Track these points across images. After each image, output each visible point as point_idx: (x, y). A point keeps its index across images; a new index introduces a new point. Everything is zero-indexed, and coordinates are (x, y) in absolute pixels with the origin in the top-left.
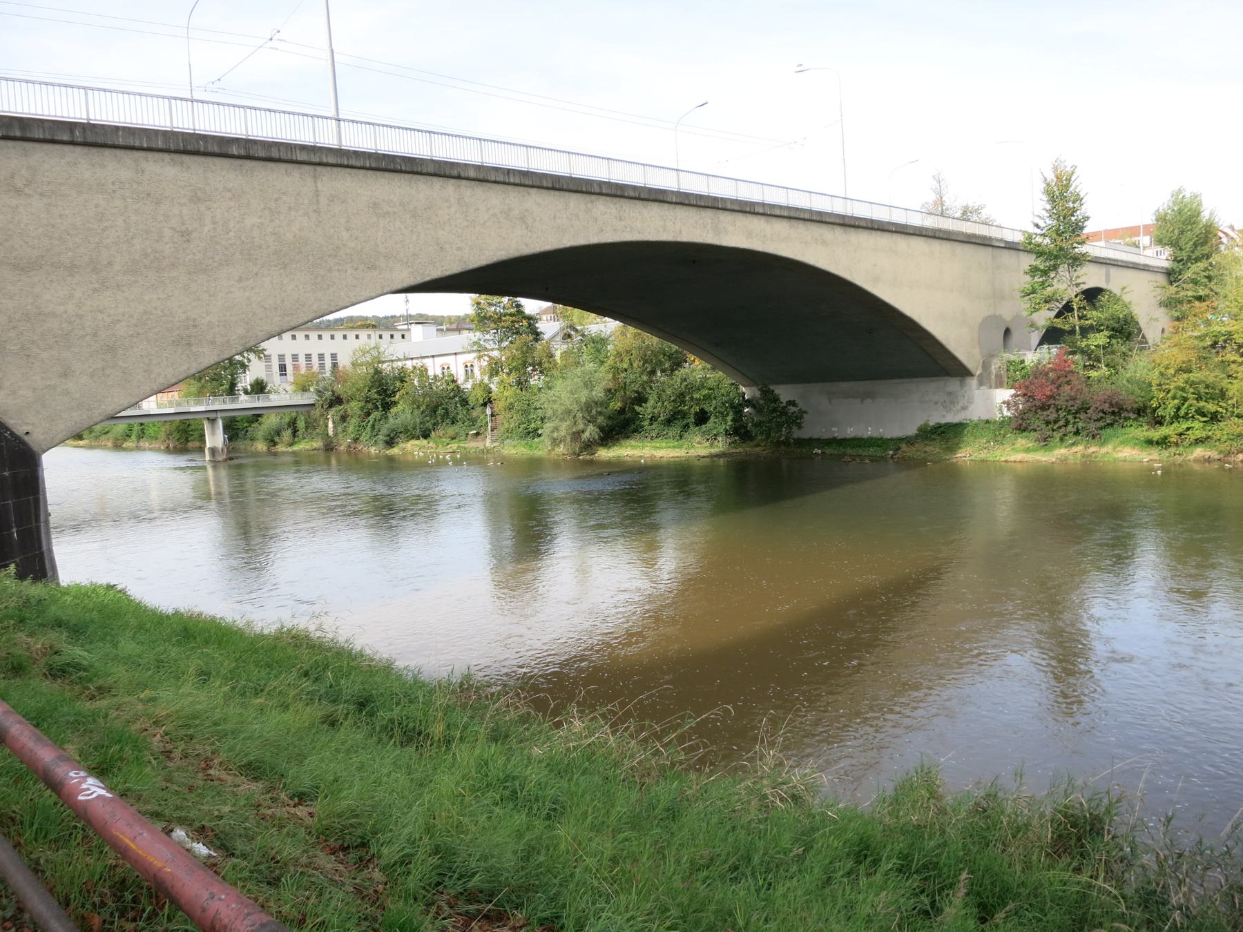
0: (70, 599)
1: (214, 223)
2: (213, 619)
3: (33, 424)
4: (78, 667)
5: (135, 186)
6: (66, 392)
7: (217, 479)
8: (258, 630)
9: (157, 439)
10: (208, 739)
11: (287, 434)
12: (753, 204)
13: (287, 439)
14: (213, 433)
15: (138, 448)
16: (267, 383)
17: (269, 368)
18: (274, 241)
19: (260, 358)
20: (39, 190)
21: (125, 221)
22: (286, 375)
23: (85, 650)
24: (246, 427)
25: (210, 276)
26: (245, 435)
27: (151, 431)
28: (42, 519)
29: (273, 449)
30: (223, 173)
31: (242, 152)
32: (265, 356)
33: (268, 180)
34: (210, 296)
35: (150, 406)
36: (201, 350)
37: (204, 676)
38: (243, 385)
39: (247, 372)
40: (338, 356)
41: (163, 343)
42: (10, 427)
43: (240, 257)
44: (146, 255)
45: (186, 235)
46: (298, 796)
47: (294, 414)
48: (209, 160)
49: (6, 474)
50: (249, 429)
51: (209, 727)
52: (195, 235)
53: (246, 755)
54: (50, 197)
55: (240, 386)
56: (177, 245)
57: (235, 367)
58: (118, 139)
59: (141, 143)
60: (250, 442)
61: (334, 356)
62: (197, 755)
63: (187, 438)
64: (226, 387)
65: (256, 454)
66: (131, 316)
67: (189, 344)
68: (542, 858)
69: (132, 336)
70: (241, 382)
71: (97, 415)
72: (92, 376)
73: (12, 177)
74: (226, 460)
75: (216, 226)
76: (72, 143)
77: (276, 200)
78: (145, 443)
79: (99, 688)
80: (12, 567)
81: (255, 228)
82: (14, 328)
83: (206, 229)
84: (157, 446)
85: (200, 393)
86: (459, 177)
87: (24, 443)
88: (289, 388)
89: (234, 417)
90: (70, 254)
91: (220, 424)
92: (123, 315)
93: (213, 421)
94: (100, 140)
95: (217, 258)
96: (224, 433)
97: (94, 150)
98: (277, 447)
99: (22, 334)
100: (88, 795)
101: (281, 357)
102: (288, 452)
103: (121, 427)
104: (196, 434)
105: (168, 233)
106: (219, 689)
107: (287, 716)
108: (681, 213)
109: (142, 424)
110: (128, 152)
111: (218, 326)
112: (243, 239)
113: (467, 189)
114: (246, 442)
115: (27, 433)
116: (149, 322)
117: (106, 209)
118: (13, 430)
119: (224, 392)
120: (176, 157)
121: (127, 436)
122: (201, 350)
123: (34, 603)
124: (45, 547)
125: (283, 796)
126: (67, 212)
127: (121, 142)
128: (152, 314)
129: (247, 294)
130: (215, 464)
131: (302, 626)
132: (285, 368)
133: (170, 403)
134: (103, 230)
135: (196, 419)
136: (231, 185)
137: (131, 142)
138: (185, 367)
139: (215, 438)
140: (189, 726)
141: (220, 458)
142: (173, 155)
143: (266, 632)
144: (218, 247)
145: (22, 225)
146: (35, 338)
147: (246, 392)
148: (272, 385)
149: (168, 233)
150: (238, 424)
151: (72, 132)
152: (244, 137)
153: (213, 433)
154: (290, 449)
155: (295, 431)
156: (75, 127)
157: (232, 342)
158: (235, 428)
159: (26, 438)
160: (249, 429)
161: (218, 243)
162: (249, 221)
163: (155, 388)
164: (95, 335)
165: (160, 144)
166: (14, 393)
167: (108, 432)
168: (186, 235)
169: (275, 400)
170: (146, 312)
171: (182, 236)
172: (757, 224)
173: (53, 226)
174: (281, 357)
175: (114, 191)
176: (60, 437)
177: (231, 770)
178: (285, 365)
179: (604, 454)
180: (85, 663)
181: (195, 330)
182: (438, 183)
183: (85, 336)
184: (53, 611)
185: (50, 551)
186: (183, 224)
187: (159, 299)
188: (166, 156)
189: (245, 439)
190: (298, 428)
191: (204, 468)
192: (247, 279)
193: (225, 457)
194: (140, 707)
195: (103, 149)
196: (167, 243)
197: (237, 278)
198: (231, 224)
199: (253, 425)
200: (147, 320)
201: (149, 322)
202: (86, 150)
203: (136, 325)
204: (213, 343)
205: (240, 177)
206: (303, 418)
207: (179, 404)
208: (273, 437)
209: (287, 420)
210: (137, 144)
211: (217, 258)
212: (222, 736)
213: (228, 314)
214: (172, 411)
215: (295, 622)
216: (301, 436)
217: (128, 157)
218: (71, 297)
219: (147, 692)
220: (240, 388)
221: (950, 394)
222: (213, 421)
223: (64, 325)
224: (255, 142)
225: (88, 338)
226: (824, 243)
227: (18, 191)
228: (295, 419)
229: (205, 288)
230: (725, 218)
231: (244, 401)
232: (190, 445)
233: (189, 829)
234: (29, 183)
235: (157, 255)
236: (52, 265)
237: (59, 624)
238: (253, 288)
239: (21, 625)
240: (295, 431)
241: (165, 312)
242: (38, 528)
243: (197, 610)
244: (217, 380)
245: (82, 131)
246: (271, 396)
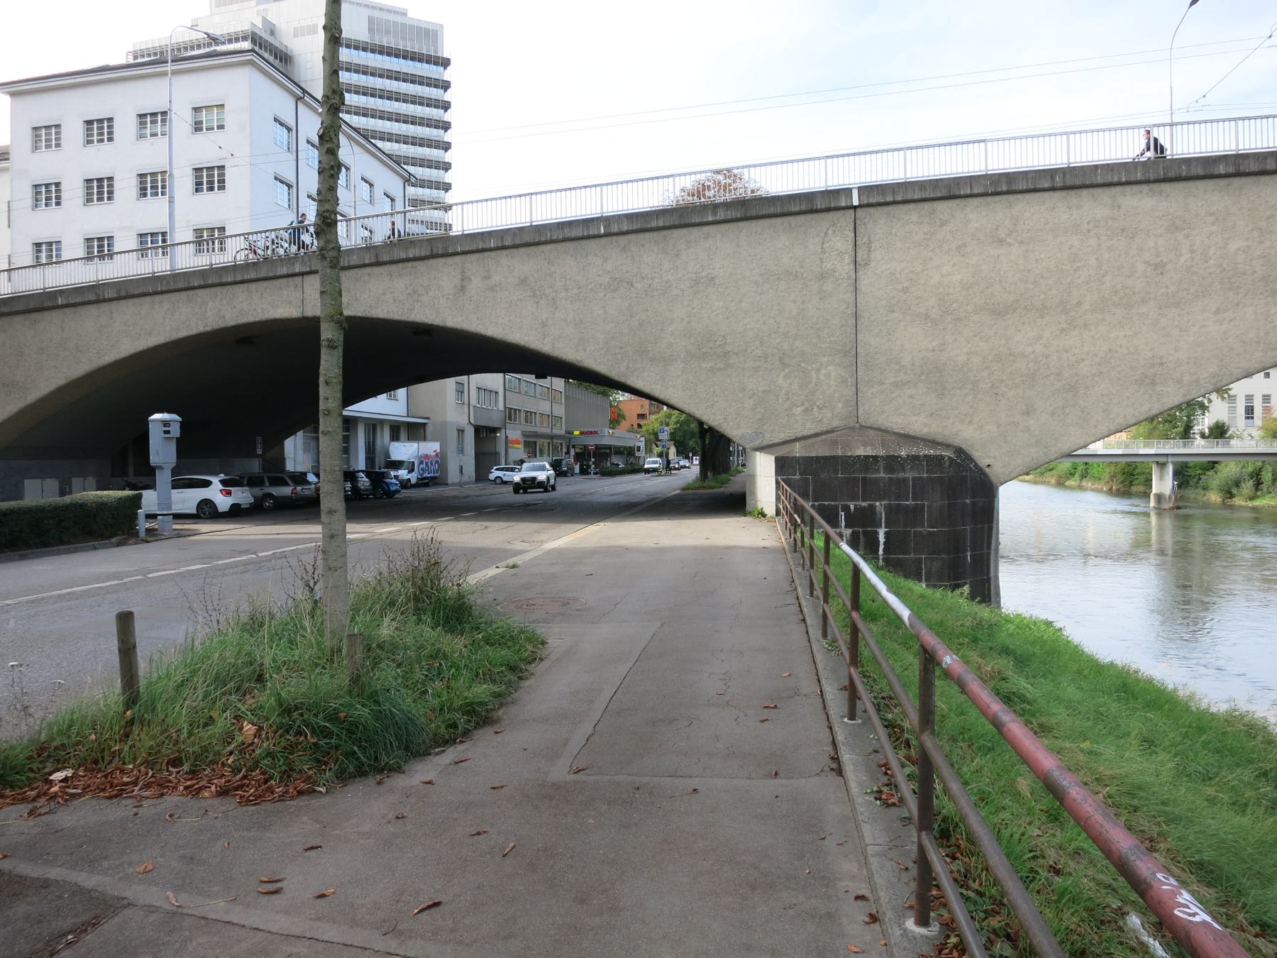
0: (1013, 627)
1: (1192, 252)
2: (1150, 681)
3: (994, 458)
4: (1023, 699)
5: (1110, 222)
6: (1028, 429)
7: (1160, 529)
8: (1204, 705)
9: (1100, 479)
10: (1154, 817)
11: (1248, 486)
13: (1248, 491)
14: (1161, 478)
15: (1081, 488)
16: (1229, 427)
17: (1232, 410)
18: (1262, 265)
19: (1223, 398)
20: (1020, 238)
21: (1097, 259)
22: (1252, 418)
23: (1029, 683)
24: (1199, 475)
25: (1183, 310)
26: (1197, 483)
27: (1094, 471)
28: (993, 547)
29: (1229, 502)
30: (1206, 197)
31: (1231, 170)
32: (1229, 396)
33: (1260, 196)
34: (1181, 331)
35: (1098, 447)
36: (1165, 389)
37: (1149, 744)
38: (1200, 428)
39: (1207, 414)
40: (1272, 398)
41: (1125, 382)
42: (975, 459)
43: (1219, 287)
44: (1116, 292)
46: (1260, 926)
47: (1259, 464)
48: (1191, 184)
49: (968, 501)
50: (1202, 477)
51: (1157, 804)
52: (1170, 266)
53: (1199, 851)
54: (1028, 244)
55: (1196, 429)
56: (1149, 279)
57: (1194, 407)
58: (1096, 177)
59: (1120, 178)
60: (1202, 492)
62: (1141, 831)
63: (1131, 482)
64: (1180, 429)
65: (1206, 505)
66: (1096, 355)
67: (1153, 383)
69: (1094, 375)
70: (1198, 424)
71: (1053, 452)
72: (1052, 414)
73: (997, 229)
74: (1173, 508)
75: (1194, 255)
76: (1053, 189)
77: (1269, 218)
78: (1087, 483)
79: (1041, 725)
80: (966, 589)
81: (1240, 252)
82: (987, 368)
83: (1182, 259)
84: (1100, 487)
85: (1149, 435)
87: (986, 475)
88: (1256, 433)
89: (1186, 463)
90: (1042, 296)
91: (1170, 468)
92: (1088, 354)
93: (1162, 466)
94: (1078, 182)
95: (1193, 290)
96: (1174, 479)
97: (1072, 193)
98: (1234, 499)
99: (993, 373)
100: (1190, 915)
101: (1249, 398)
102: (1247, 507)
103: (1066, 465)
104: (1142, 478)
105: (1140, 267)
106: (1165, 763)
107: (1246, 821)
109: (1086, 464)
110: (1106, 189)
111: (1188, 363)
112: (1225, 265)
114: (1197, 491)
115: (989, 466)
116: (1113, 361)
117: (1079, 250)
118: (978, 462)
119: (1177, 434)
120: (1155, 186)
121: (1071, 474)
122: (1165, 389)
123: (986, 626)
124: (992, 574)
125: (1241, 917)
126: (1043, 256)
127: (1099, 180)
128: (1116, 352)
129: (1224, 327)
130: (1160, 512)
131: (1259, 715)
132: (1253, 410)
133: (1119, 444)
134: (1076, 271)
135: (1143, 462)
136: (1215, 208)
137: (1109, 179)
138: (1145, 408)
139: (1163, 484)
140: (1133, 796)
141: (1167, 505)
142: (1152, 186)
143: (1214, 710)
144: (1194, 278)
145: (1002, 273)
146: (1004, 377)
147: (1203, 436)
148: (1235, 429)
149: (1140, 267)
150: (1190, 470)
151: (1053, 178)
152: (1234, 153)
153: (1161, 478)
154: (1250, 504)
155: (1258, 485)
156: (1056, 173)
157: (1202, 382)
158: (1186, 475)
159: (987, 470)
160: (1202, 477)
161: (1196, 273)
162: (1233, 247)
163: (1113, 428)
164: (1058, 374)
165: (1139, 176)
166: (981, 428)
167: (1052, 469)
169: (1236, 446)
170: (1110, 351)
171: (1155, 269)
173: (1029, 271)
174: (1249, 398)
175: (1089, 231)
176: (1017, 471)
177: (1179, 862)
178: (1252, 407)
180: (1028, 695)
181: (1161, 369)
183: (1049, 375)
184: (1002, 637)
185: (997, 577)
186: (1158, 256)
187: (1125, 336)
188: (1145, 188)
189: (1196, 488)
190: (1263, 480)
191: (1147, 515)
192: (1226, 311)
193: (1171, 505)
194: (1081, 757)
195: (1080, 190)
196: (1139, 278)
197: (1214, 309)
198: (1212, 251)
199: (1208, 473)
200: (1111, 358)
201: (1113, 361)
202: (1064, 193)
203: (1099, 364)
204: (1179, 381)
205: (1226, 198)
206: (1270, 469)
207: (1127, 446)
208: (1230, 488)
209: (1250, 469)
210: (1116, 179)
211: (1193, 290)
212: (1173, 820)
213: (1200, 349)
214: (1120, 452)
215: (1251, 708)
216: (1265, 490)
217: (1104, 195)
218: (1040, 337)
219: (1088, 743)
220: (1196, 431)
222: (1162, 466)
223: (1031, 365)
224: (1246, 156)
225: (1052, 377)
227: (1001, 241)
228: (1260, 470)
229: (1176, 323)
231: (1199, 446)
232: (1134, 489)
233: (1145, 919)
234: (1011, 233)
235: (1127, 291)
236: (1025, 308)
237: (1005, 651)
238: (1231, 321)
239: (973, 644)
240: (1258, 485)
241: (1131, 349)
242: (989, 554)
243: (1134, 667)
244: (1171, 422)
245: (1062, 176)
246: (1233, 442)
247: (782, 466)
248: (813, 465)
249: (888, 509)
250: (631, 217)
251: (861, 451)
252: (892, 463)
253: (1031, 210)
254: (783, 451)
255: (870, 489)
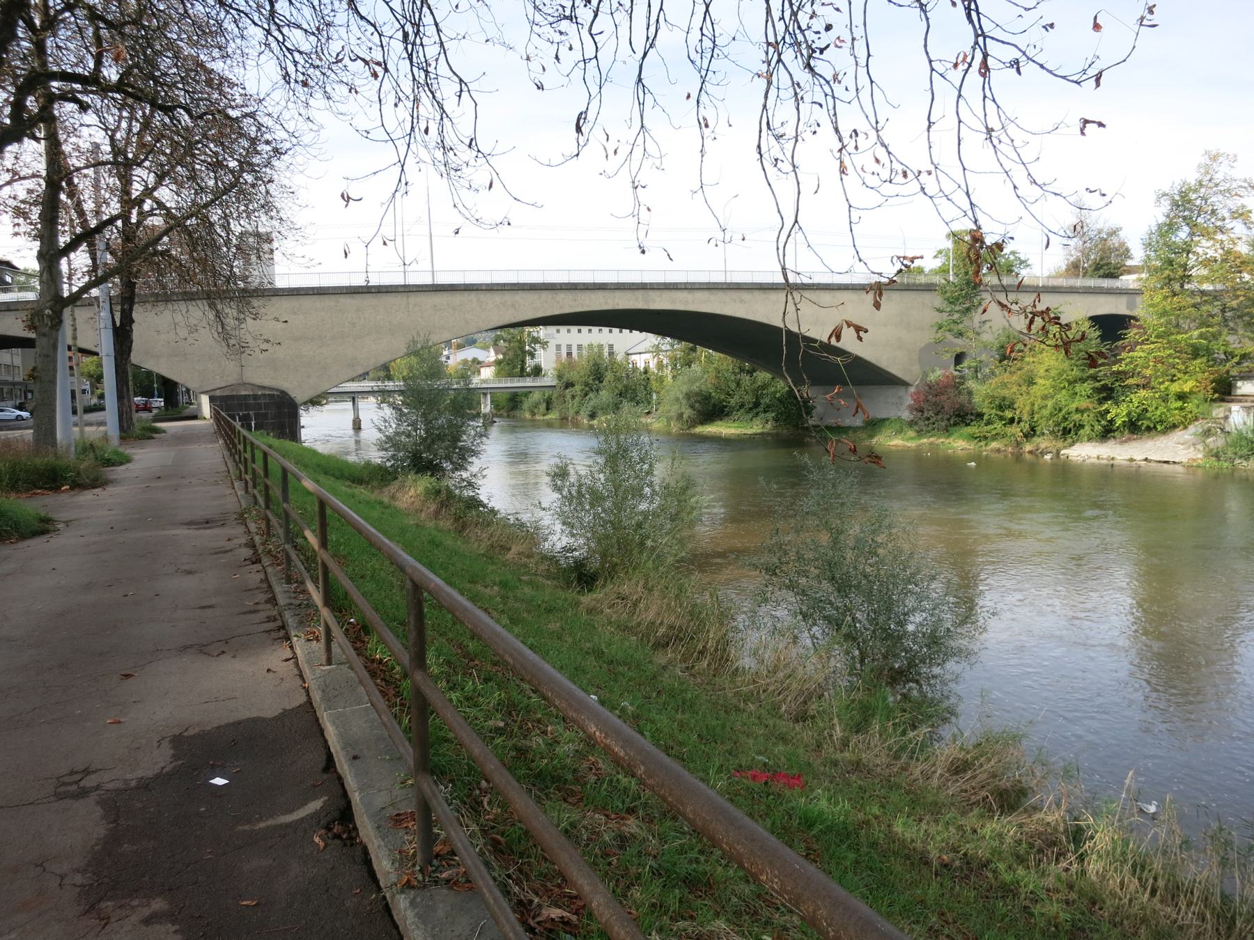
12: (676, 284)
45: (354, 325)
61: (611, 346)
68: (919, 892)
86: (477, 290)
108: (618, 294)
113: (483, 296)
168: (354, 325)
172: (667, 295)
174: (569, 347)
179: (700, 429)
182: (466, 293)
221: (900, 397)
226: (742, 301)
230: (652, 294)
247: (212, 399)
248: (224, 399)
249: (255, 415)
250: (584, 284)
251: (243, 393)
252: (255, 397)
253: (307, 302)
254: (212, 394)
255: (248, 407)
